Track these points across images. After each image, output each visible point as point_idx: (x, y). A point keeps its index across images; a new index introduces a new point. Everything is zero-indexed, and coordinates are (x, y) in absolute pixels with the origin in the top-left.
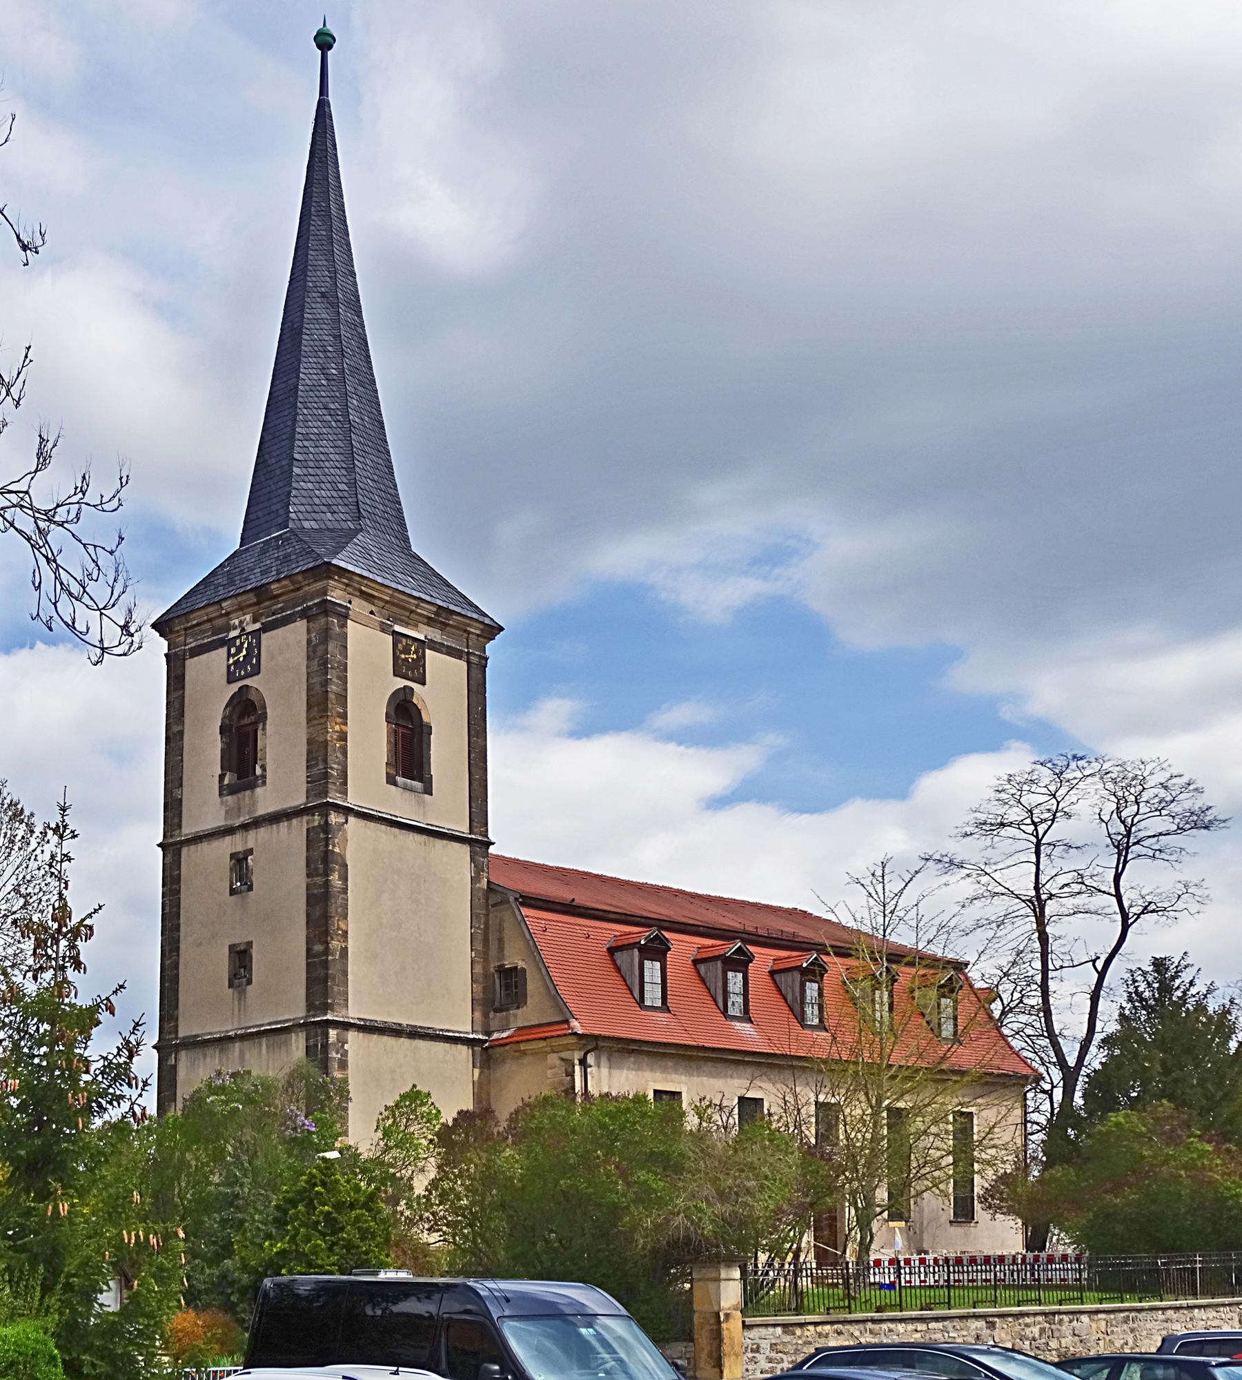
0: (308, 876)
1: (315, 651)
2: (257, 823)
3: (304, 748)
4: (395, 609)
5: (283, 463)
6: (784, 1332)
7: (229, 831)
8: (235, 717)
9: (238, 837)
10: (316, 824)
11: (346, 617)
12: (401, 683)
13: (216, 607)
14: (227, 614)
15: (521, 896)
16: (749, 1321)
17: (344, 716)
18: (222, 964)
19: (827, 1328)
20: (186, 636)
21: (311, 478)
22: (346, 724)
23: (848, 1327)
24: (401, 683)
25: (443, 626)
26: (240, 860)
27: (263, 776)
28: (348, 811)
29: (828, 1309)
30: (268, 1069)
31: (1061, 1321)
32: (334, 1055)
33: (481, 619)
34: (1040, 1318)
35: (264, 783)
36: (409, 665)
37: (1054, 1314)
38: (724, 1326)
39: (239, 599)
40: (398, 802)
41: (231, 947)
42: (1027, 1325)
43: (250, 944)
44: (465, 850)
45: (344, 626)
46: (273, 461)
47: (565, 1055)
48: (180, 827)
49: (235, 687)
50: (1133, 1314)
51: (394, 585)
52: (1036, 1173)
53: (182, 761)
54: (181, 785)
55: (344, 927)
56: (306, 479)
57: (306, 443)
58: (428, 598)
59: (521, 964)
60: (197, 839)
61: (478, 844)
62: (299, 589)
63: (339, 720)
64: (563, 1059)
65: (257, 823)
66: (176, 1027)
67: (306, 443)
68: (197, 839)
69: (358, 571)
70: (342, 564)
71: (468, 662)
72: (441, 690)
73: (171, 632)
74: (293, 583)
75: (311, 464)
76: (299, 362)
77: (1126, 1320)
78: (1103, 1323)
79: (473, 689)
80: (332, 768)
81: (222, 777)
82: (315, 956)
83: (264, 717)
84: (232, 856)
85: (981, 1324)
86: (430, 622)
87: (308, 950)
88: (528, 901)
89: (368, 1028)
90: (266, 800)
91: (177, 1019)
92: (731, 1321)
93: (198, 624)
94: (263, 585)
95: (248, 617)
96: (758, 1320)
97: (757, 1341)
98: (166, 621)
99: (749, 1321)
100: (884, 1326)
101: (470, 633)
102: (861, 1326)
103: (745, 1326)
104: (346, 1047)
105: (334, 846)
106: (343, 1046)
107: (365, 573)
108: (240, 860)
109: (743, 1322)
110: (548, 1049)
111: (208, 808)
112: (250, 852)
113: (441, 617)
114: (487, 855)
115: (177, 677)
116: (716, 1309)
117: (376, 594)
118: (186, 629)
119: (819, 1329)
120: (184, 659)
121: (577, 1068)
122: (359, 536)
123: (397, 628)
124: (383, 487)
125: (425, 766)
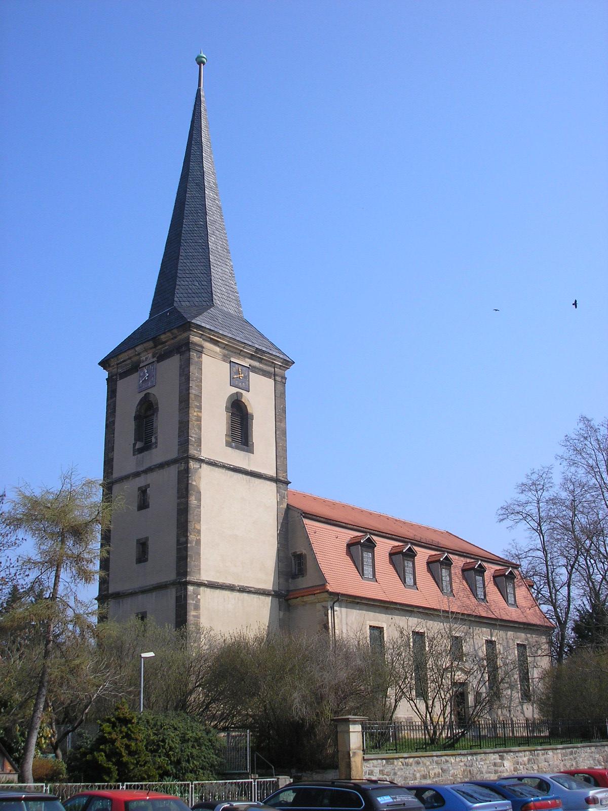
0: (179, 498)
1: (183, 371)
2: (150, 470)
3: (177, 426)
4: (231, 349)
5: (173, 272)
6: (387, 763)
7: (137, 474)
8: (143, 411)
9: (143, 477)
10: (182, 468)
11: (201, 352)
12: (235, 390)
13: (133, 350)
14: (139, 354)
15: (304, 513)
16: (366, 757)
17: (200, 408)
18: (132, 551)
19: (411, 760)
20: (117, 368)
21: (187, 279)
22: (201, 412)
23: (423, 759)
24: (235, 390)
25: (260, 360)
26: (143, 491)
27: (156, 443)
28: (202, 461)
29: (416, 749)
30: (491, 636)
31: (538, 754)
32: (191, 602)
33: (281, 356)
34: (527, 753)
35: (156, 447)
36: (239, 379)
37: (534, 750)
38: (352, 759)
39: (145, 345)
40: (237, 458)
41: (138, 541)
42: (521, 757)
43: (147, 539)
44: (273, 486)
45: (200, 357)
46: (168, 271)
47: (324, 604)
48: (112, 474)
49: (142, 395)
50: (575, 749)
51: (230, 335)
52: (93, 641)
53: (114, 437)
54: (113, 451)
55: (198, 528)
56: (184, 279)
57: (185, 261)
58: (250, 343)
59: (304, 552)
60: (122, 479)
61: (280, 481)
62: (175, 337)
63: (196, 410)
64: (323, 607)
65: (150, 470)
66: (108, 587)
67: (185, 261)
68: (122, 479)
69: (208, 327)
70: (199, 323)
71: (275, 380)
72: (260, 396)
73: (109, 366)
74: (172, 334)
75: (187, 272)
76: (183, 218)
77: (571, 753)
78: (560, 755)
79: (278, 395)
80: (191, 437)
81: (135, 445)
82: (181, 544)
83: (156, 410)
84: (139, 489)
85: (497, 756)
86: (252, 357)
87: (178, 541)
88: (307, 515)
89: (212, 586)
90: (157, 456)
91: (108, 583)
92: (357, 757)
93: (123, 362)
94: (156, 337)
95: (150, 355)
96: (372, 756)
97: (372, 768)
98: (106, 361)
99: (366, 757)
100: (443, 759)
101: (274, 365)
102: (431, 759)
103: (364, 759)
104: (199, 597)
105: (193, 481)
106: (197, 596)
107: (212, 328)
108: (143, 491)
109: (363, 757)
110: (316, 600)
111: (126, 463)
112: (148, 486)
113: (257, 355)
114: (286, 490)
115: (281, 421)
116: (349, 750)
117: (219, 340)
118: (118, 364)
119: (407, 760)
120: (116, 381)
121: (330, 611)
122: (212, 309)
123: (233, 360)
124: (228, 284)
125: (249, 438)
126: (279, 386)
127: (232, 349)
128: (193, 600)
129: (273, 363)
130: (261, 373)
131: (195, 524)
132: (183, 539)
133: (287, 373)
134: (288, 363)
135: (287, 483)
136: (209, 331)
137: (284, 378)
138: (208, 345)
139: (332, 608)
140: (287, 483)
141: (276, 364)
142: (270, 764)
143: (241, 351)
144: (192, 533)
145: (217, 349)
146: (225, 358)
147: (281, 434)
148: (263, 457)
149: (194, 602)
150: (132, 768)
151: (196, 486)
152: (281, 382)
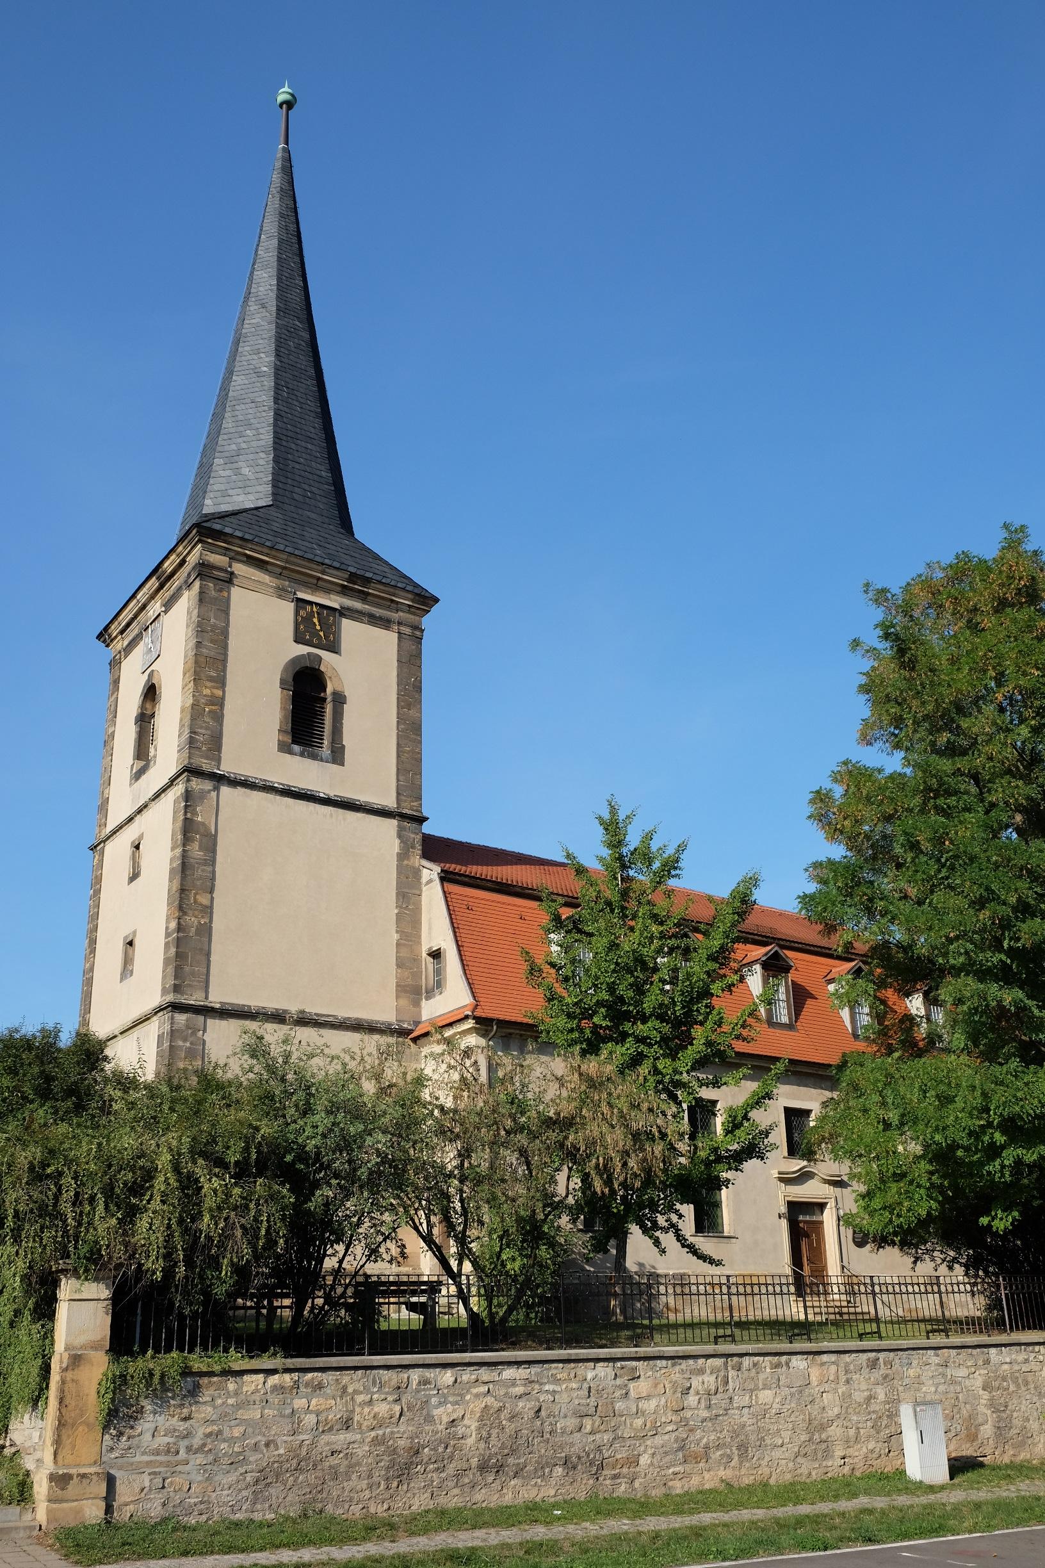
25: (364, 597)
36: (315, 627)
40: (301, 771)
86: (344, 591)
101: (400, 601)
123: (300, 595)
126: (409, 645)
127: (298, 576)
128: (185, 1040)
129: (392, 601)
130: (366, 619)
131: (196, 894)
132: (209, 650)
133: (426, 621)
134: (425, 601)
135: (421, 820)
136: (240, 543)
137: (417, 628)
138: (239, 568)
139: (169, 1273)
140: (421, 820)
141: (398, 603)
142: (139, 1311)
143: (319, 579)
144: (190, 912)
145: (266, 578)
146: (281, 593)
147: (410, 731)
148: (368, 755)
149: (188, 1044)
150: (485, 1165)
151: (203, 824)
152: (413, 636)
